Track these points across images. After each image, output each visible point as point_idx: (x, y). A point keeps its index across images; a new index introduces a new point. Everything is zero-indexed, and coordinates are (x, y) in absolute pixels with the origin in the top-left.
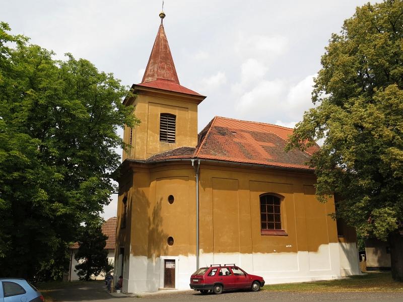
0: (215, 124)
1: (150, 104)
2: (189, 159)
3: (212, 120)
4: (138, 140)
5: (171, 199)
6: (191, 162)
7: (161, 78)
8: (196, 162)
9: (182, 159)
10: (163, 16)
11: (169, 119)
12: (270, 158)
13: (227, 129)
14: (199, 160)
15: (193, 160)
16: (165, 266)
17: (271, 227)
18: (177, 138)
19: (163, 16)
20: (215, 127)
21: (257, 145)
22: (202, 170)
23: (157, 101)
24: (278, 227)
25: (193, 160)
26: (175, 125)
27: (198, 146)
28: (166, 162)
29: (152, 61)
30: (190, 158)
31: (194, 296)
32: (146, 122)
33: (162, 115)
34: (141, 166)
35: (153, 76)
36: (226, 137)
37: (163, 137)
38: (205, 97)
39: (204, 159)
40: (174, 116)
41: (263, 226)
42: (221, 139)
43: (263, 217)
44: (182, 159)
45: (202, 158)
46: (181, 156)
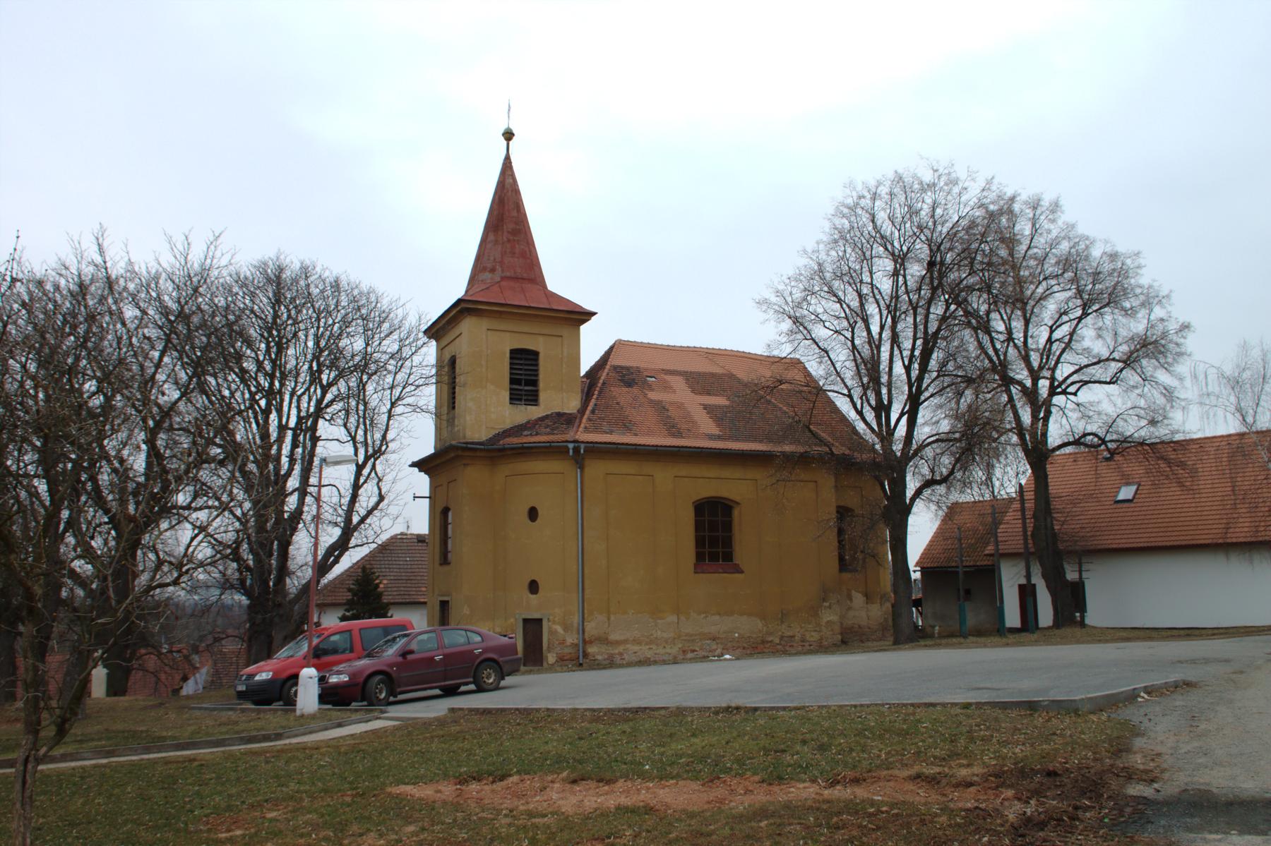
0: (613, 361)
1: (489, 332)
2: (565, 444)
3: (612, 348)
4: (470, 404)
5: (533, 514)
6: (568, 449)
7: (508, 274)
8: (576, 450)
9: (553, 444)
10: (509, 135)
11: (526, 359)
12: (716, 431)
13: (638, 370)
14: (582, 446)
15: (571, 446)
16: (1013, 631)
17: (714, 557)
18: (543, 396)
19: (509, 135)
20: (615, 368)
21: (693, 404)
22: (587, 462)
23: (502, 327)
24: (728, 557)
25: (571, 446)
26: (537, 370)
27: (582, 411)
28: (523, 448)
29: (491, 237)
30: (567, 441)
31: (223, 229)
32: (484, 370)
33: (513, 352)
34: (478, 454)
35: (493, 270)
36: (635, 390)
37: (515, 398)
38: (594, 314)
39: (591, 443)
40: (536, 354)
41: (700, 557)
42: (622, 394)
43: (700, 542)
44: (553, 444)
45: (588, 442)
46: (551, 438)
